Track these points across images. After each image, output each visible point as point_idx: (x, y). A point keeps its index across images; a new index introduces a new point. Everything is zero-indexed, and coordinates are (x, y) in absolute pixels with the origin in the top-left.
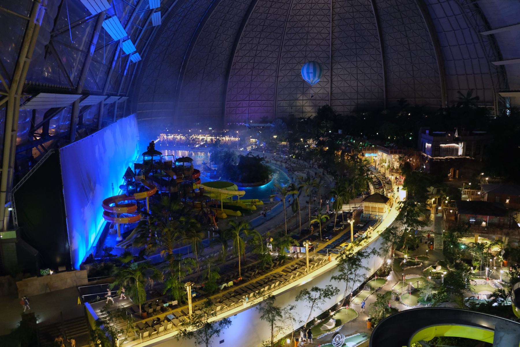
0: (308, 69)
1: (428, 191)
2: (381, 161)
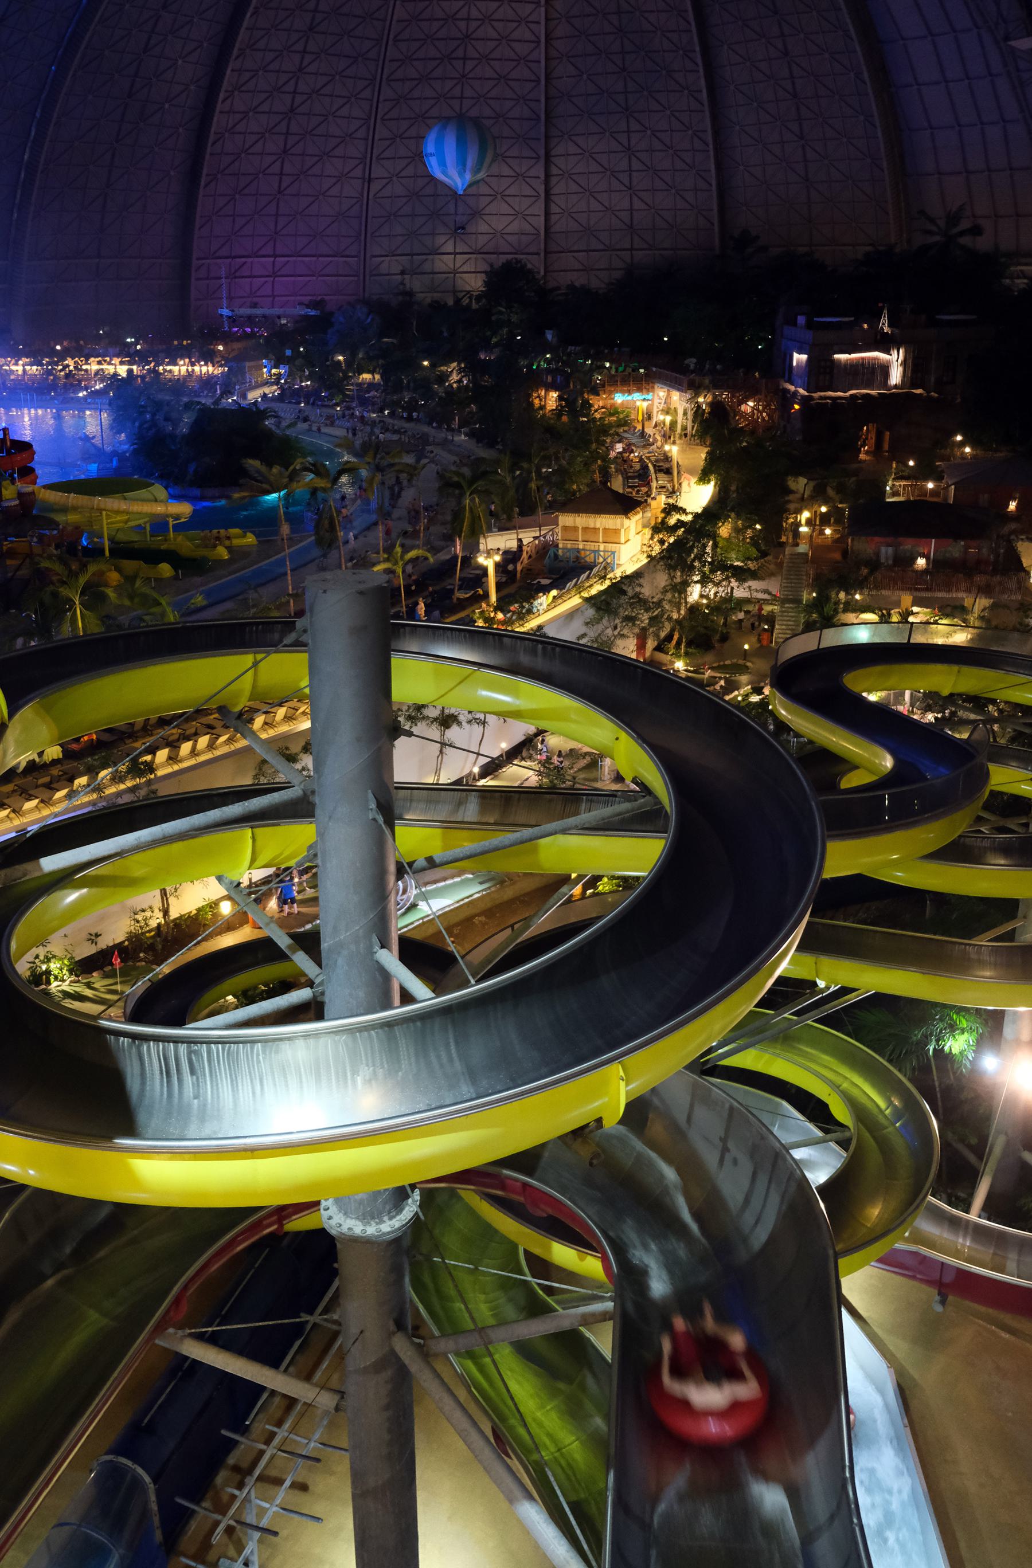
0: (439, 142)
1: (792, 492)
2: (659, 407)
